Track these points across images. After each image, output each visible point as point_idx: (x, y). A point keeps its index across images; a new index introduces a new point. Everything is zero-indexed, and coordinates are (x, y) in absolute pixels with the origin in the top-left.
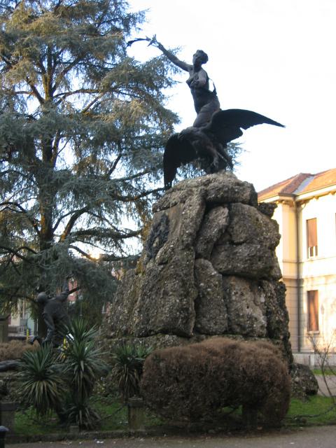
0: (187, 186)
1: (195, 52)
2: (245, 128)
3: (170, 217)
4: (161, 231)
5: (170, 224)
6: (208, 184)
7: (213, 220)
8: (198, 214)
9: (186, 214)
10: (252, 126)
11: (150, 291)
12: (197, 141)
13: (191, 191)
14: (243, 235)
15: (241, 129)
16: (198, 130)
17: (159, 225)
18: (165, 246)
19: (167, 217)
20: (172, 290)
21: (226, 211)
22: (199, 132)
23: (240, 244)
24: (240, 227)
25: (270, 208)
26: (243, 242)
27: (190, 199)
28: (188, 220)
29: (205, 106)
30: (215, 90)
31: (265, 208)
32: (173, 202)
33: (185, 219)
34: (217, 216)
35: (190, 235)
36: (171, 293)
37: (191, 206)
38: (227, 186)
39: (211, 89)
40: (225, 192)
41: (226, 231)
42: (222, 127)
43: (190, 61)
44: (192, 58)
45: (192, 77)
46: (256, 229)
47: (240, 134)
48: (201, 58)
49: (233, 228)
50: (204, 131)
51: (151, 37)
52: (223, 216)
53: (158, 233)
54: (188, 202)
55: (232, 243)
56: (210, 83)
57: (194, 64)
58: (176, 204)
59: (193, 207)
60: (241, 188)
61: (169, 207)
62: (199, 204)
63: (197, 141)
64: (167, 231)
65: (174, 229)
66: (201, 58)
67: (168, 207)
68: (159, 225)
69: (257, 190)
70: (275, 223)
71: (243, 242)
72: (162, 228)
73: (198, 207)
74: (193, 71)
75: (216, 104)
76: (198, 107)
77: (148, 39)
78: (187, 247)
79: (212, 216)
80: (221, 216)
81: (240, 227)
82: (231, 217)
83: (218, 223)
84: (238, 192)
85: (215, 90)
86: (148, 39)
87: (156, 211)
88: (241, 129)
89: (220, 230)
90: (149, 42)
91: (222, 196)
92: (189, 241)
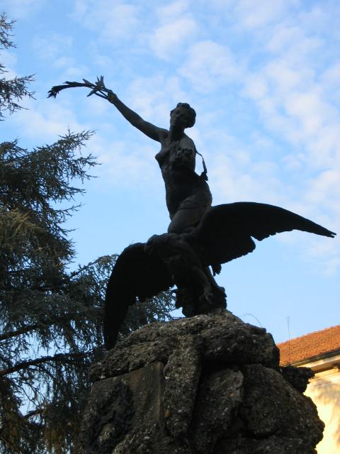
0: (158, 335)
1: (174, 107)
2: (260, 239)
3: (134, 387)
4: (115, 412)
5: (134, 398)
6: (199, 331)
7: (218, 392)
8: (193, 380)
9: (173, 379)
12: (178, 257)
13: (176, 340)
14: (271, 421)
15: (253, 239)
16: (179, 239)
17: (110, 402)
18: (128, 440)
19: (128, 388)
21: (240, 376)
22: (181, 242)
23: (266, 436)
24: (265, 405)
25: (301, 376)
26: (271, 434)
27: (178, 354)
28: (179, 391)
29: (187, 199)
30: (204, 173)
31: (294, 376)
32: (137, 361)
33: (172, 388)
34: (226, 386)
35: (184, 416)
37: (180, 366)
38: (244, 333)
39: (198, 171)
40: (241, 342)
41: (240, 412)
42: (209, 230)
43: (164, 123)
44: (169, 118)
45: (167, 149)
46: (288, 411)
47: (251, 247)
48: (184, 116)
49: (250, 408)
50: (187, 239)
51: (93, 81)
52: (236, 386)
53: (110, 416)
54: (172, 360)
55: (249, 435)
56: (198, 159)
57: (172, 127)
58: (141, 365)
59: (184, 367)
60: (262, 338)
61: (127, 371)
62: (195, 363)
63: (178, 257)
64: (129, 412)
65: (146, 407)
66: (184, 116)
67: (125, 371)
68: (110, 402)
69: (278, 340)
70: (309, 400)
71: (271, 434)
72: (116, 406)
73: (193, 368)
74: (168, 141)
75: (207, 196)
76: (173, 203)
77: (87, 84)
78: (180, 440)
79: (216, 385)
80: (232, 386)
81: (265, 405)
82: (247, 387)
83: (230, 398)
84: (256, 345)
85: (204, 173)
86: (87, 84)
87: (98, 380)
88: (253, 239)
89: (232, 410)
90: (90, 90)
91: (236, 350)
92: (184, 429)
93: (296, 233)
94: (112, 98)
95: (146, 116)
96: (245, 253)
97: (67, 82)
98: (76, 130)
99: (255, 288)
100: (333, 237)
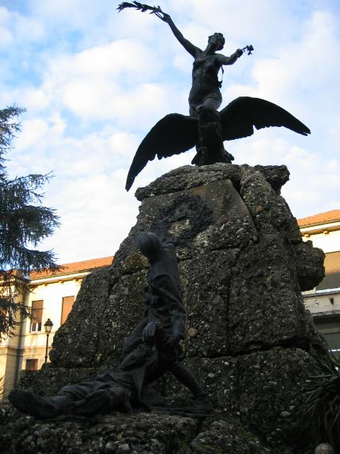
2: (258, 128)
10: (268, 126)
11: (221, 284)
15: (254, 126)
20: (283, 280)
36: (283, 284)
39: (220, 80)
43: (203, 45)
47: (251, 133)
58: (201, 184)
76: (195, 98)
88: (254, 126)
93: (283, 131)
94: (167, 18)
95: (186, 36)
96: (245, 136)
97: (135, 2)
98: (19, 105)
99: (252, 150)
100: (307, 135)
